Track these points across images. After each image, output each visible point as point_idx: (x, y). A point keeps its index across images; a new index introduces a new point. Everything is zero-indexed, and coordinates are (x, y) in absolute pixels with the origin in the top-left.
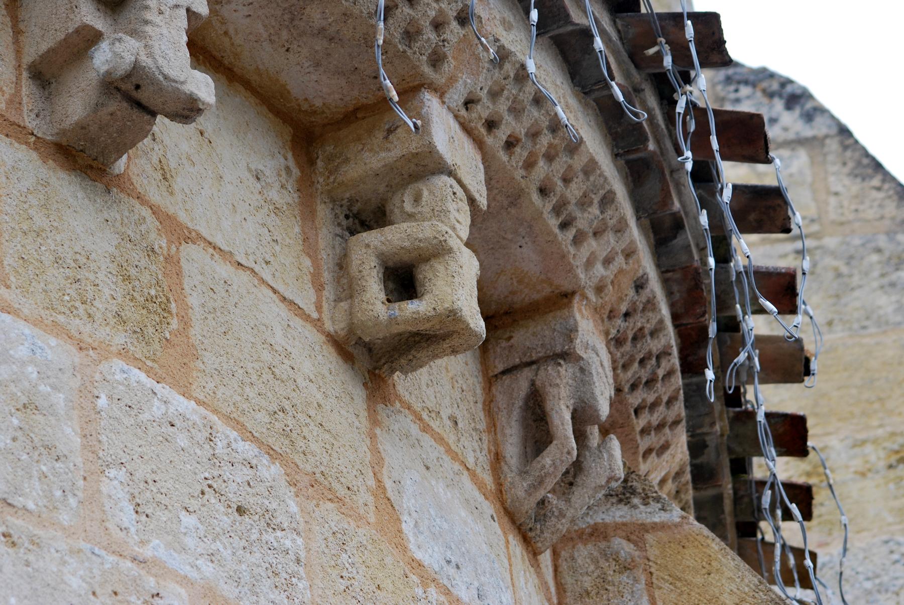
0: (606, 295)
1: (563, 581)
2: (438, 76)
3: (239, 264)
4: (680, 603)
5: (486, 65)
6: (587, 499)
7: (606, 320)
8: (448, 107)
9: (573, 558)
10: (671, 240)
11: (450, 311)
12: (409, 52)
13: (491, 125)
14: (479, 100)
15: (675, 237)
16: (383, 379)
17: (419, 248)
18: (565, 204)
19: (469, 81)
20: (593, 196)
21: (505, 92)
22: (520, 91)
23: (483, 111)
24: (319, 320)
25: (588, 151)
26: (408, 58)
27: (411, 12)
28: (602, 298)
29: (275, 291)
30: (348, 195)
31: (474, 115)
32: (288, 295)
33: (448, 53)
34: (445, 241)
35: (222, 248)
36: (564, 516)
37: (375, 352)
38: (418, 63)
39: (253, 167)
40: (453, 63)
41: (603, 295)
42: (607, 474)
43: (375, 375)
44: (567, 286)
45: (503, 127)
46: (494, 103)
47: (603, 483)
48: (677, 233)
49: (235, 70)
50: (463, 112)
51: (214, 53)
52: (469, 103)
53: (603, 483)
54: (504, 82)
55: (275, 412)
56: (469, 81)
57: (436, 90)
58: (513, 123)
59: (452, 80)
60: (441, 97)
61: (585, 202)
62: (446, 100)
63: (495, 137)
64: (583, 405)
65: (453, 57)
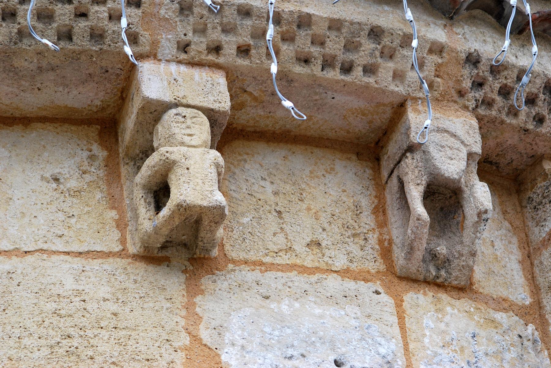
0: (439, 87)
1: (538, 283)
2: (141, 48)
3: (26, 252)
4: (281, 366)
5: (177, 19)
6: (473, 235)
7: (458, 100)
8: (166, 61)
9: (541, 263)
10: (503, 13)
11: (178, 206)
12: (105, 47)
13: (217, 49)
14: (190, 42)
15: (504, 9)
16: (204, 258)
17: (156, 171)
18: (334, 58)
19: (169, 36)
20: (358, 39)
21: (209, 25)
22: (222, 18)
23: (199, 45)
24: (123, 250)
25: (322, 18)
26: (106, 51)
27: (87, 23)
28: (436, 90)
29: (68, 253)
30: (138, 152)
31: (192, 54)
32: (84, 248)
33: (137, 30)
34: (167, 158)
35: (6, 250)
36: (462, 255)
37: (189, 244)
38: (118, 50)
39: (48, 175)
40: (146, 34)
41: (435, 88)
42: (475, 212)
43: (195, 259)
44: (397, 100)
45: (225, 46)
46: (205, 36)
47: (477, 219)
48: (502, 6)
49: (28, 116)
50: (183, 56)
51: (4, 115)
52: (184, 47)
53: (477, 219)
54: (202, 20)
55: (59, 343)
56: (169, 36)
57: (148, 56)
58: (234, 39)
59: (155, 44)
60: (155, 57)
61: (351, 46)
62: (160, 58)
63: (225, 55)
64: (433, 176)
65: (145, 30)
